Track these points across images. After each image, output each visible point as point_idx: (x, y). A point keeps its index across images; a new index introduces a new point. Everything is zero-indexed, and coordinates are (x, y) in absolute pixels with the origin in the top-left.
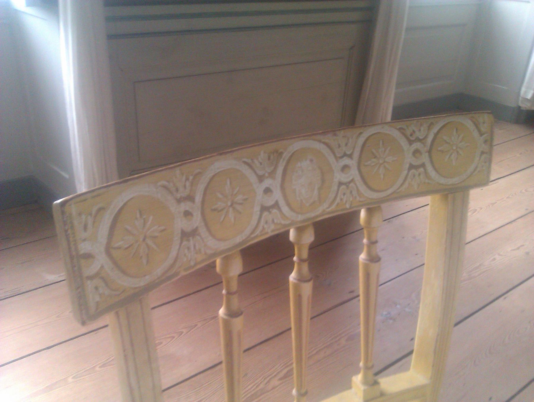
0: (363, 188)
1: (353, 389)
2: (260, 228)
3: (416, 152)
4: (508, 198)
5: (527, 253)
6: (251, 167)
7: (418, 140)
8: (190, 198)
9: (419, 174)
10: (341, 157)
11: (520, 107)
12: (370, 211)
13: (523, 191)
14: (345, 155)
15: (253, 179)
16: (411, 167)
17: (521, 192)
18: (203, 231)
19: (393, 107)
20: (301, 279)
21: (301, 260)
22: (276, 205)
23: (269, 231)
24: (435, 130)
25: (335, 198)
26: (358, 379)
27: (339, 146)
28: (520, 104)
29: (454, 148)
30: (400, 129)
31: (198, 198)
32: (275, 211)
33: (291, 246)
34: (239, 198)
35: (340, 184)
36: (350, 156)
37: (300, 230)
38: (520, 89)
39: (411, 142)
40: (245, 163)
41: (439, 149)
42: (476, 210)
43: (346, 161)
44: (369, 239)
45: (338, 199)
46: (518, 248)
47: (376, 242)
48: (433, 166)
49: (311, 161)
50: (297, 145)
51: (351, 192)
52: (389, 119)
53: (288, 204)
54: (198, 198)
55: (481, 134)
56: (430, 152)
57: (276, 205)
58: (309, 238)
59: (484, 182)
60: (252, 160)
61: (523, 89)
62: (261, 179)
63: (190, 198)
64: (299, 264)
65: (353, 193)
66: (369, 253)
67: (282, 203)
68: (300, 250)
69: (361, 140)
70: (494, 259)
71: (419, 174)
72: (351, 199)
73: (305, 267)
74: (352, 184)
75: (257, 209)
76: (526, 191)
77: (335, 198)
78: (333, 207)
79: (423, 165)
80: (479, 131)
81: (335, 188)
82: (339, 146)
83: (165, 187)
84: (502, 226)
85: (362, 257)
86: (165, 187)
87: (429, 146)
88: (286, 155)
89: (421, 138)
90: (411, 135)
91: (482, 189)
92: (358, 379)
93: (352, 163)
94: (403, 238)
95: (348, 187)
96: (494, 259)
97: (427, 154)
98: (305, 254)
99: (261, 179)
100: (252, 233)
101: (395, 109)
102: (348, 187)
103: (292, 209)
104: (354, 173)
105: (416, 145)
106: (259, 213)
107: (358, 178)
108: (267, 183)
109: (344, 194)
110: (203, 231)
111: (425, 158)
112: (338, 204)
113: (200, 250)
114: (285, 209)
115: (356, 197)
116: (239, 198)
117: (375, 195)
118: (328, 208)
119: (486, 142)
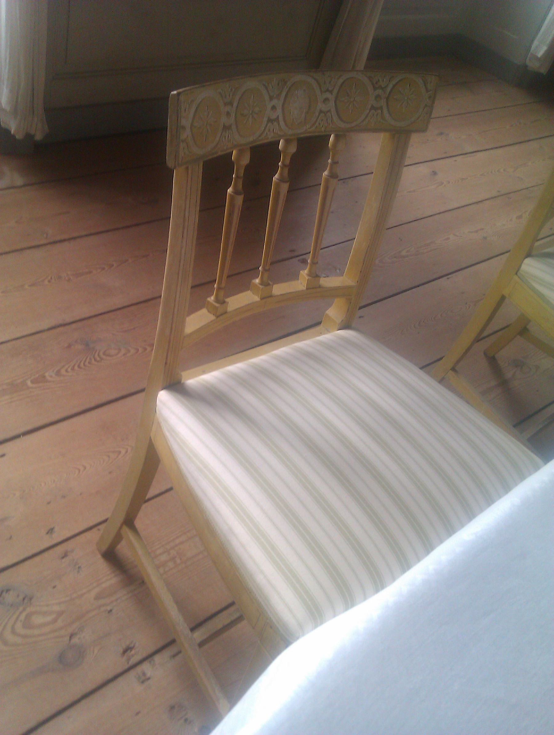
0: (335, 118)
1: (299, 281)
2: (265, 134)
3: (378, 97)
4: (482, 175)
5: (485, 238)
6: (267, 88)
7: (381, 87)
8: (231, 104)
9: (377, 114)
10: (325, 92)
11: (526, 66)
12: (337, 137)
13: (502, 170)
14: (328, 90)
15: (267, 97)
16: (373, 108)
17: (499, 171)
18: (234, 127)
19: (373, 37)
20: (281, 180)
21: (284, 165)
22: (277, 119)
23: (270, 137)
24: (394, 82)
25: (316, 122)
26: (304, 273)
27: (325, 83)
28: (528, 63)
29: (406, 98)
30: (370, 78)
31: (235, 104)
32: (275, 123)
33: (279, 153)
34: (257, 109)
35: (321, 112)
36: (331, 92)
37: (287, 141)
38: (532, 41)
39: (375, 89)
40: (264, 85)
41: (395, 97)
42: (442, 183)
43: (328, 95)
44: (333, 159)
45: (317, 124)
46: (476, 232)
47: (337, 163)
48: (388, 110)
49: (304, 91)
50: (298, 77)
51: (327, 120)
52: (362, 68)
53: (285, 121)
54: (235, 104)
55: (427, 90)
56: (387, 99)
57: (277, 119)
58: (293, 149)
59: (423, 130)
60: (268, 84)
61: (536, 43)
62: (271, 98)
63: (231, 104)
64: (282, 168)
65: (328, 120)
66: (331, 171)
67: (281, 119)
68: (284, 157)
69: (341, 81)
70: (448, 239)
71: (377, 114)
72: (326, 125)
73: (286, 171)
74: (329, 114)
75: (265, 119)
76: (504, 170)
77: (316, 122)
78: (313, 128)
79: (381, 108)
80: (426, 89)
81: (317, 114)
82: (325, 83)
83: (220, 93)
84: (468, 205)
85: (326, 173)
86: (220, 93)
87: (388, 93)
88: (289, 84)
89: (383, 86)
90: (376, 83)
91: (456, 161)
92: (304, 273)
93: (332, 97)
94: (357, 202)
95: (325, 115)
96: (448, 239)
97: (385, 100)
98: (288, 162)
99: (271, 98)
100: (260, 136)
101: (376, 42)
102: (325, 115)
103: (286, 125)
104: (332, 104)
105: (379, 92)
106: (266, 122)
107: (333, 110)
108: (274, 102)
109: (322, 120)
110: (234, 127)
111: (383, 103)
112: (317, 127)
113: (230, 140)
114: (282, 123)
115: (329, 124)
116: (257, 109)
117: (342, 125)
118: (309, 129)
119: (430, 97)
